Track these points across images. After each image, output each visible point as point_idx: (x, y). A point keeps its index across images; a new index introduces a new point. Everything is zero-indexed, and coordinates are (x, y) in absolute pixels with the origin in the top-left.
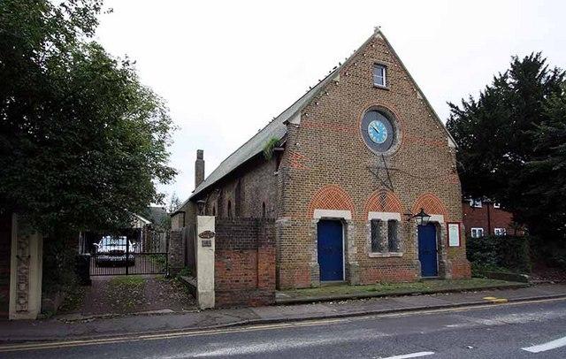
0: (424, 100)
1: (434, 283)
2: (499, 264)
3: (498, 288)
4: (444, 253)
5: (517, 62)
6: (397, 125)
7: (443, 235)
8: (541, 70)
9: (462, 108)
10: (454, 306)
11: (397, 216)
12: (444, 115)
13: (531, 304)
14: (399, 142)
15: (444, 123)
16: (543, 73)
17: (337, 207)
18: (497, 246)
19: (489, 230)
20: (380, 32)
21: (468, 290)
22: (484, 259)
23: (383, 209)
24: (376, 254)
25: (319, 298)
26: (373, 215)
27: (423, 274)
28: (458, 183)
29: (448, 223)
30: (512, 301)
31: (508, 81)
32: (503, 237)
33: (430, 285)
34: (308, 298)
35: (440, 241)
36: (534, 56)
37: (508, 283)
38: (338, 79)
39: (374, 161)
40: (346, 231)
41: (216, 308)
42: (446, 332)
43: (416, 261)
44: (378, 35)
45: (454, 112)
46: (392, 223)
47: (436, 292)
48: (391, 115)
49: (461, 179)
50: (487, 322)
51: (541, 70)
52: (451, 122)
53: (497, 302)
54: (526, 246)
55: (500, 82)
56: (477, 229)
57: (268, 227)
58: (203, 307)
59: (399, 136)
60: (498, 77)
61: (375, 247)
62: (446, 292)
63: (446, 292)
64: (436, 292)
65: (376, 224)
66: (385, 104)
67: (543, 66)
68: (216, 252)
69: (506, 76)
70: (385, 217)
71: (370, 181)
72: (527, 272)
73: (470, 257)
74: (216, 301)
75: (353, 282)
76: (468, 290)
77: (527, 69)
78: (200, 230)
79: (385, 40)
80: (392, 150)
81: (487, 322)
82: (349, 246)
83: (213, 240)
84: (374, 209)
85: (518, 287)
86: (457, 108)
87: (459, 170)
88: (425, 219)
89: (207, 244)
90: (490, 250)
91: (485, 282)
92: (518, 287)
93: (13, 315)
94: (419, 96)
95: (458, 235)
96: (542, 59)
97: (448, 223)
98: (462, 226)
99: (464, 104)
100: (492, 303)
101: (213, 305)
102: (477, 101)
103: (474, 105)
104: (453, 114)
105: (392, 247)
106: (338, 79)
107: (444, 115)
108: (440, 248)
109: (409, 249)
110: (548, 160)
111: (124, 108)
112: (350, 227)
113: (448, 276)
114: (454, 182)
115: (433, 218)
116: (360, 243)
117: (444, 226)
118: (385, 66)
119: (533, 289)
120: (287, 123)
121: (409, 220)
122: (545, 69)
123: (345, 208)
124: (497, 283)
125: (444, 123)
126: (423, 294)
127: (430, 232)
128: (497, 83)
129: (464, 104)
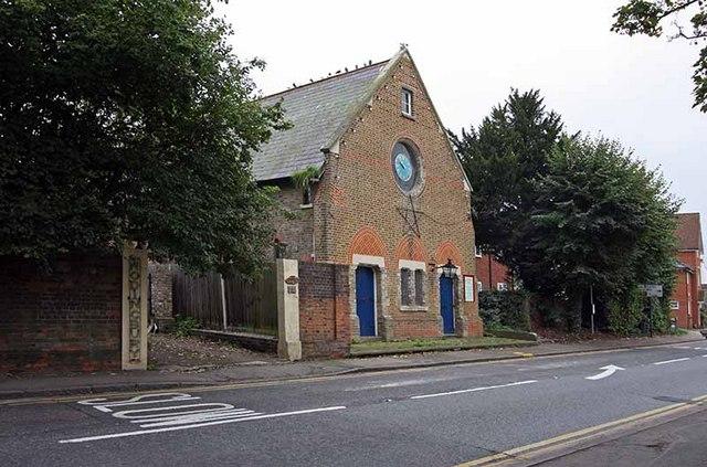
5: (516, 95)
6: (421, 161)
11: (422, 266)
17: (372, 253)
18: (500, 303)
20: (407, 52)
23: (411, 257)
24: (404, 308)
25: (385, 351)
26: (403, 264)
28: (472, 231)
32: (504, 293)
33: (452, 342)
34: (376, 351)
36: (533, 93)
37: (509, 341)
38: (370, 103)
39: (403, 202)
40: (379, 282)
41: (303, 360)
44: (405, 55)
46: (418, 272)
48: (416, 149)
55: (498, 114)
57: (343, 274)
58: (292, 359)
59: (423, 174)
61: (405, 300)
62: (479, 347)
63: (479, 347)
65: (404, 271)
66: (412, 137)
68: (300, 300)
70: (413, 265)
71: (399, 225)
74: (303, 353)
75: (388, 337)
77: (526, 105)
78: (287, 276)
79: (412, 62)
80: (416, 191)
81: (544, 367)
82: (383, 297)
83: (297, 285)
84: (403, 257)
86: (456, 137)
87: (473, 217)
89: (292, 291)
90: (493, 307)
91: (493, 341)
93: (126, 365)
101: (300, 357)
105: (419, 301)
106: (370, 103)
109: (432, 304)
110: (553, 216)
112: (383, 276)
113: (465, 334)
114: (469, 229)
116: (392, 294)
117: (461, 279)
118: (411, 92)
120: (326, 151)
127: (448, 282)
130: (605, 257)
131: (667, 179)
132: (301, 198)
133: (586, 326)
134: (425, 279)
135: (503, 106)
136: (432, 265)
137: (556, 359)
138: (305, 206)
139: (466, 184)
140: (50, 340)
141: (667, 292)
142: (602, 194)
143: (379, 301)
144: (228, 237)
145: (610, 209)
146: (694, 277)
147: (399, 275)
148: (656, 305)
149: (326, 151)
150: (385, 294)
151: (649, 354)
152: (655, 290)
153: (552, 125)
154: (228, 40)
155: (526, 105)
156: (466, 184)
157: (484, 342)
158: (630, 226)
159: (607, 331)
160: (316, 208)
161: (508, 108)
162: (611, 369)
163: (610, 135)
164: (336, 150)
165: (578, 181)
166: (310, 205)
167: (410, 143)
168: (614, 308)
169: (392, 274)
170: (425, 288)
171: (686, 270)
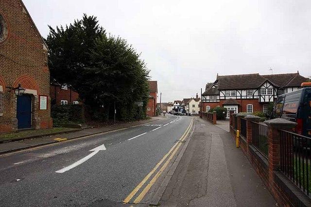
0: (28, 15)
1: (31, 132)
2: (70, 119)
3: (65, 132)
4: (36, 113)
7: (36, 102)
8: (96, 26)
9: (56, 31)
10: (32, 147)
12: (45, 33)
13: (55, 146)
14: (6, 37)
15: (46, 39)
16: (97, 28)
19: (70, 101)
21: (47, 135)
22: (62, 117)
27: (19, 128)
28: (48, 72)
29: (40, 96)
30: (69, 139)
31: (82, 25)
35: (33, 106)
36: (93, 18)
37: (71, 129)
42: (14, 168)
43: (14, 119)
45: (52, 33)
47: (24, 139)
49: (50, 70)
50: (47, 155)
51: (96, 26)
52: (50, 37)
53: (61, 141)
54: (83, 110)
55: (78, 24)
56: (64, 101)
60: (77, 22)
64: (24, 139)
67: (97, 24)
69: (80, 23)
72: (82, 123)
73: (54, 116)
76: (47, 135)
77: (90, 22)
85: (76, 131)
86: (54, 30)
88: (22, 91)
90: (66, 112)
91: (61, 129)
92: (76, 131)
94: (24, 11)
95: (46, 103)
96: (97, 20)
97: (40, 96)
98: (49, 98)
99: (58, 29)
100: (58, 142)
102: (65, 30)
103: (63, 31)
104: (51, 33)
107: (45, 33)
108: (34, 111)
111: (136, 60)
113: (38, 127)
115: (28, 91)
117: (37, 97)
119: (83, 132)
121: (10, 91)
122: (97, 26)
123: (34, 88)
124: (66, 129)
125: (46, 39)
126: (13, 141)
128: (76, 24)
129: (58, 29)
130: (118, 89)
131: (145, 62)
133: (111, 118)
137: (73, 142)
139: (44, 47)
141: (145, 105)
142: (116, 61)
145: (120, 67)
146: (155, 100)
148: (141, 110)
151: (135, 130)
152: (141, 104)
153: (101, 35)
154: (149, 75)
155: (90, 22)
156: (44, 47)
157: (55, 130)
158: (127, 75)
159: (122, 120)
162: (102, 148)
163: (123, 37)
165: (106, 53)
168: (125, 111)
171: (153, 98)
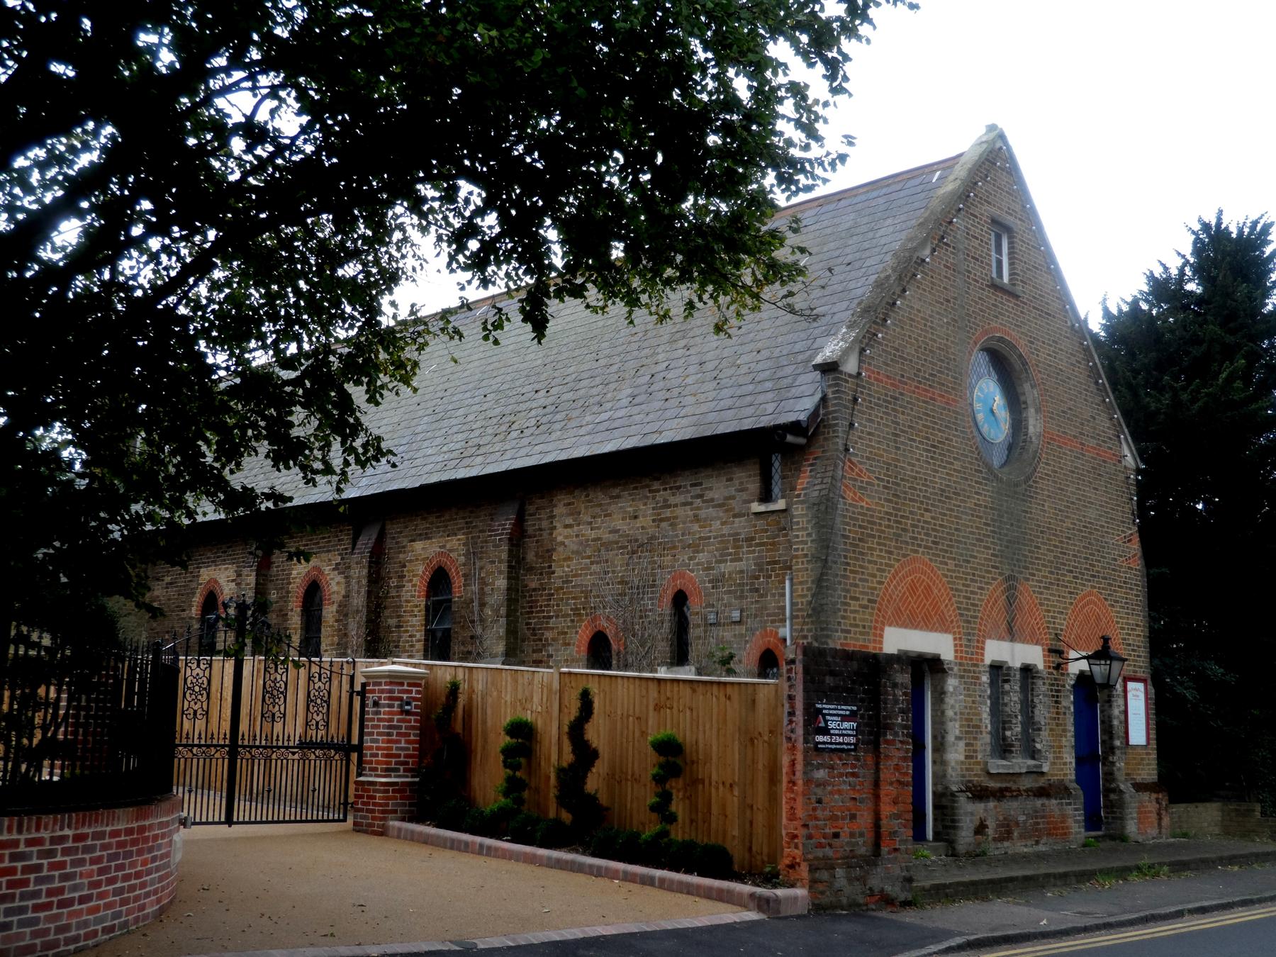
6: (1030, 393)
11: (1033, 655)
23: (1011, 633)
36: (1246, 231)
40: (940, 696)
46: (1027, 670)
48: (1017, 365)
61: (1003, 748)
65: (997, 669)
66: (1013, 335)
82: (950, 738)
112: (951, 683)
116: (971, 729)
132: (754, 486)
134: (1042, 688)
135: (1174, 272)
136: (1056, 653)
138: (762, 508)
139: (1126, 451)
140: (985, 146)
143: (940, 747)
144: (790, 300)
147: (985, 678)
149: (829, 368)
150: (954, 729)
160: (798, 511)
161: (1188, 271)
164: (851, 366)
166: (780, 504)
167: (1004, 350)
169: (968, 675)
170: (1042, 713)
